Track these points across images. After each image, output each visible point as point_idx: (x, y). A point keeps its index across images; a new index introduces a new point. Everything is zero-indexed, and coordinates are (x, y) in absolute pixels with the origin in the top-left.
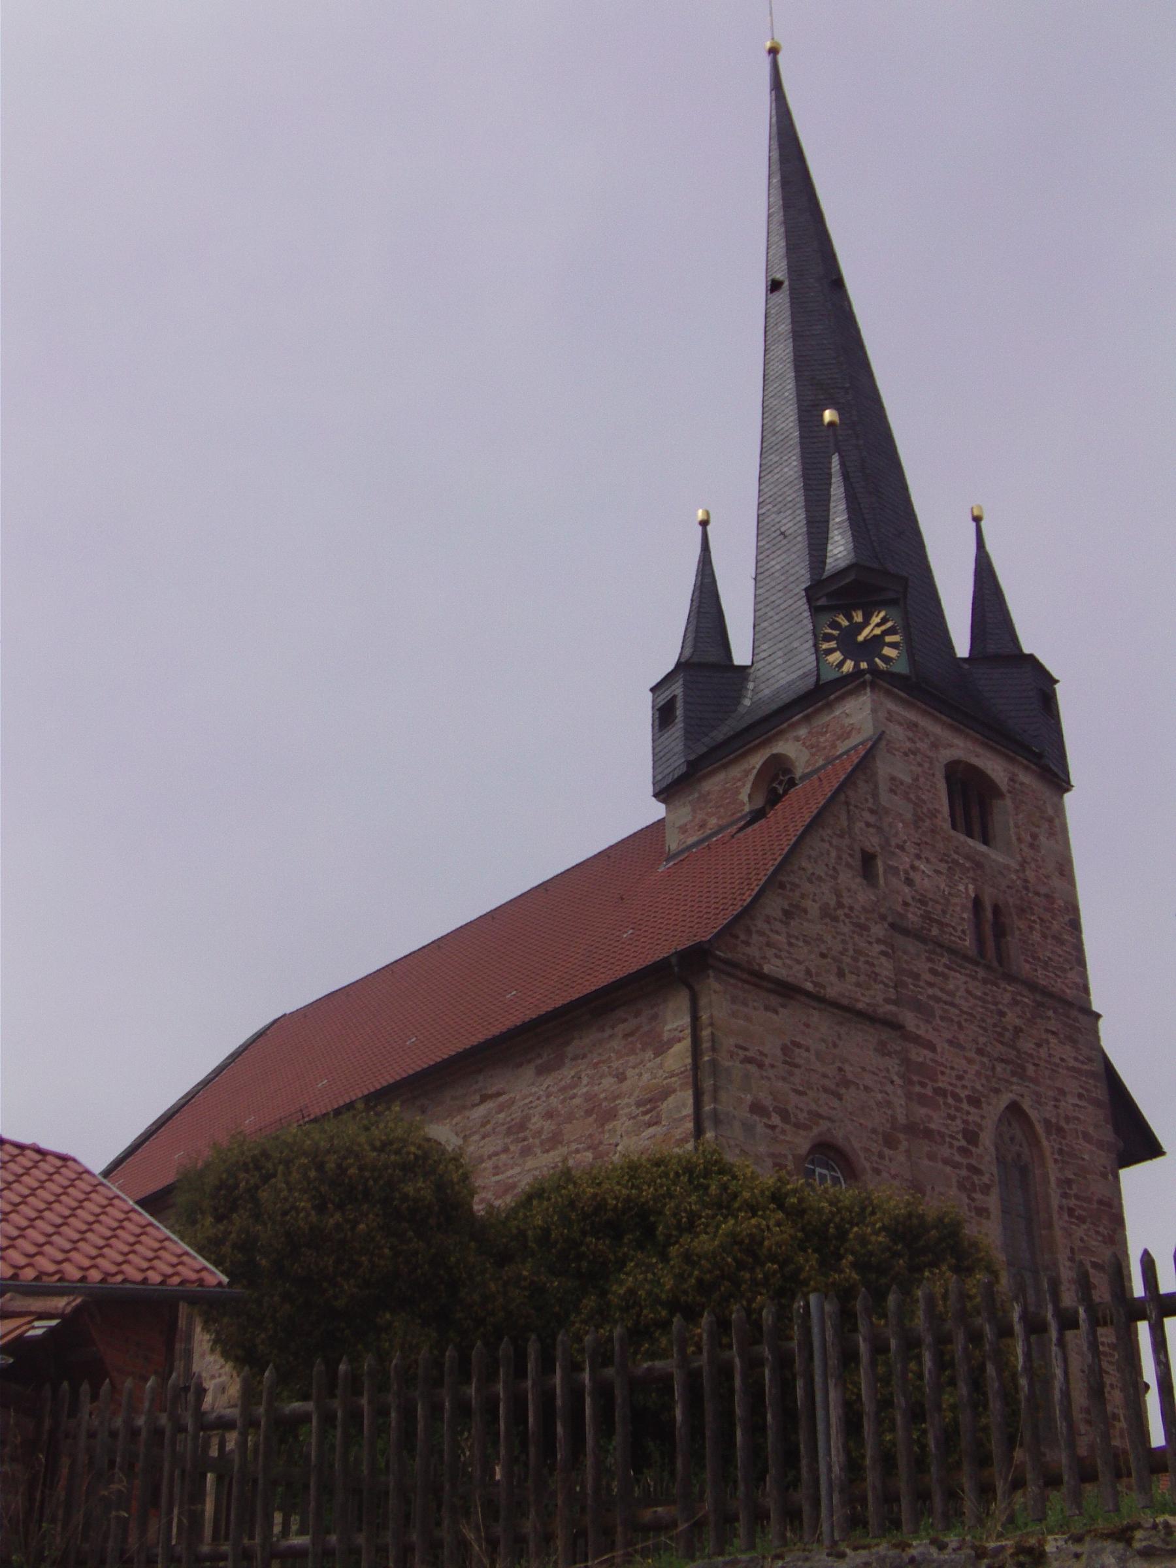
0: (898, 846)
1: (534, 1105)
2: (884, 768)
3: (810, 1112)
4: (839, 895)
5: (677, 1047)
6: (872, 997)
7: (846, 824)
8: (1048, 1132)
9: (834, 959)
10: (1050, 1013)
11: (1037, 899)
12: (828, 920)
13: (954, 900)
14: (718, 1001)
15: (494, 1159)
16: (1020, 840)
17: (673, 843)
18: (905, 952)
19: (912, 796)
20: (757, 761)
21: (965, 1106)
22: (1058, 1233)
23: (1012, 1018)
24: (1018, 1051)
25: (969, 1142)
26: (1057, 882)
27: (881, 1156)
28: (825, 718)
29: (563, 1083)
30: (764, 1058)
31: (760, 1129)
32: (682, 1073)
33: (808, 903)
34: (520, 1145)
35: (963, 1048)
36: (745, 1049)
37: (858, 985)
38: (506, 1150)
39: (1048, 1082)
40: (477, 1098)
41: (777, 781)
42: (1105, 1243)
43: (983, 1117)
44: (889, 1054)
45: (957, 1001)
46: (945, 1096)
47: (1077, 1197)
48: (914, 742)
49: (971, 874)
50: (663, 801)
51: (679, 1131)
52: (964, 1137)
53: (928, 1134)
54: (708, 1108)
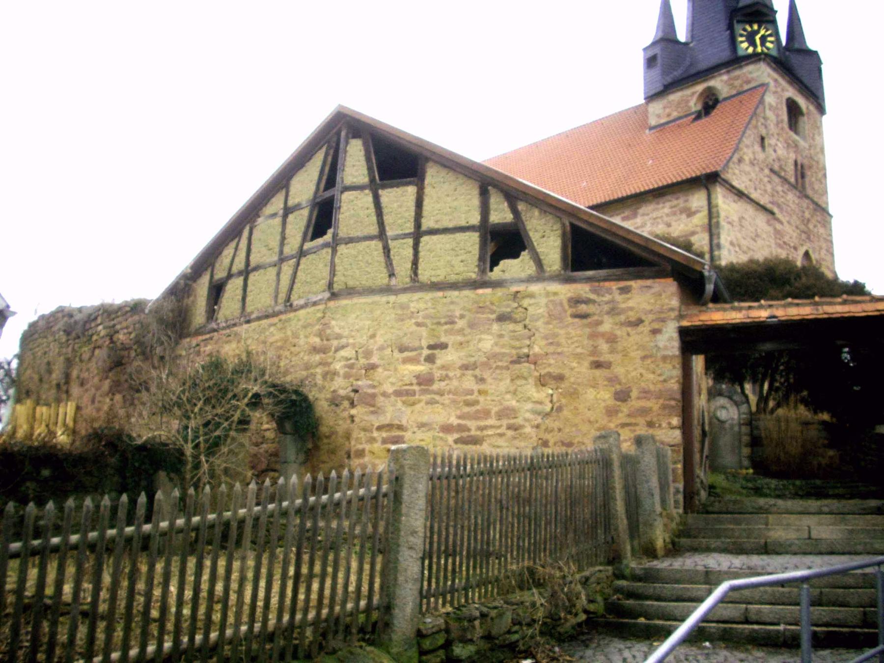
5: (698, 215)
6: (764, 200)
14: (720, 196)
23: (807, 215)
26: (828, 258)
28: (737, 73)
31: (733, 252)
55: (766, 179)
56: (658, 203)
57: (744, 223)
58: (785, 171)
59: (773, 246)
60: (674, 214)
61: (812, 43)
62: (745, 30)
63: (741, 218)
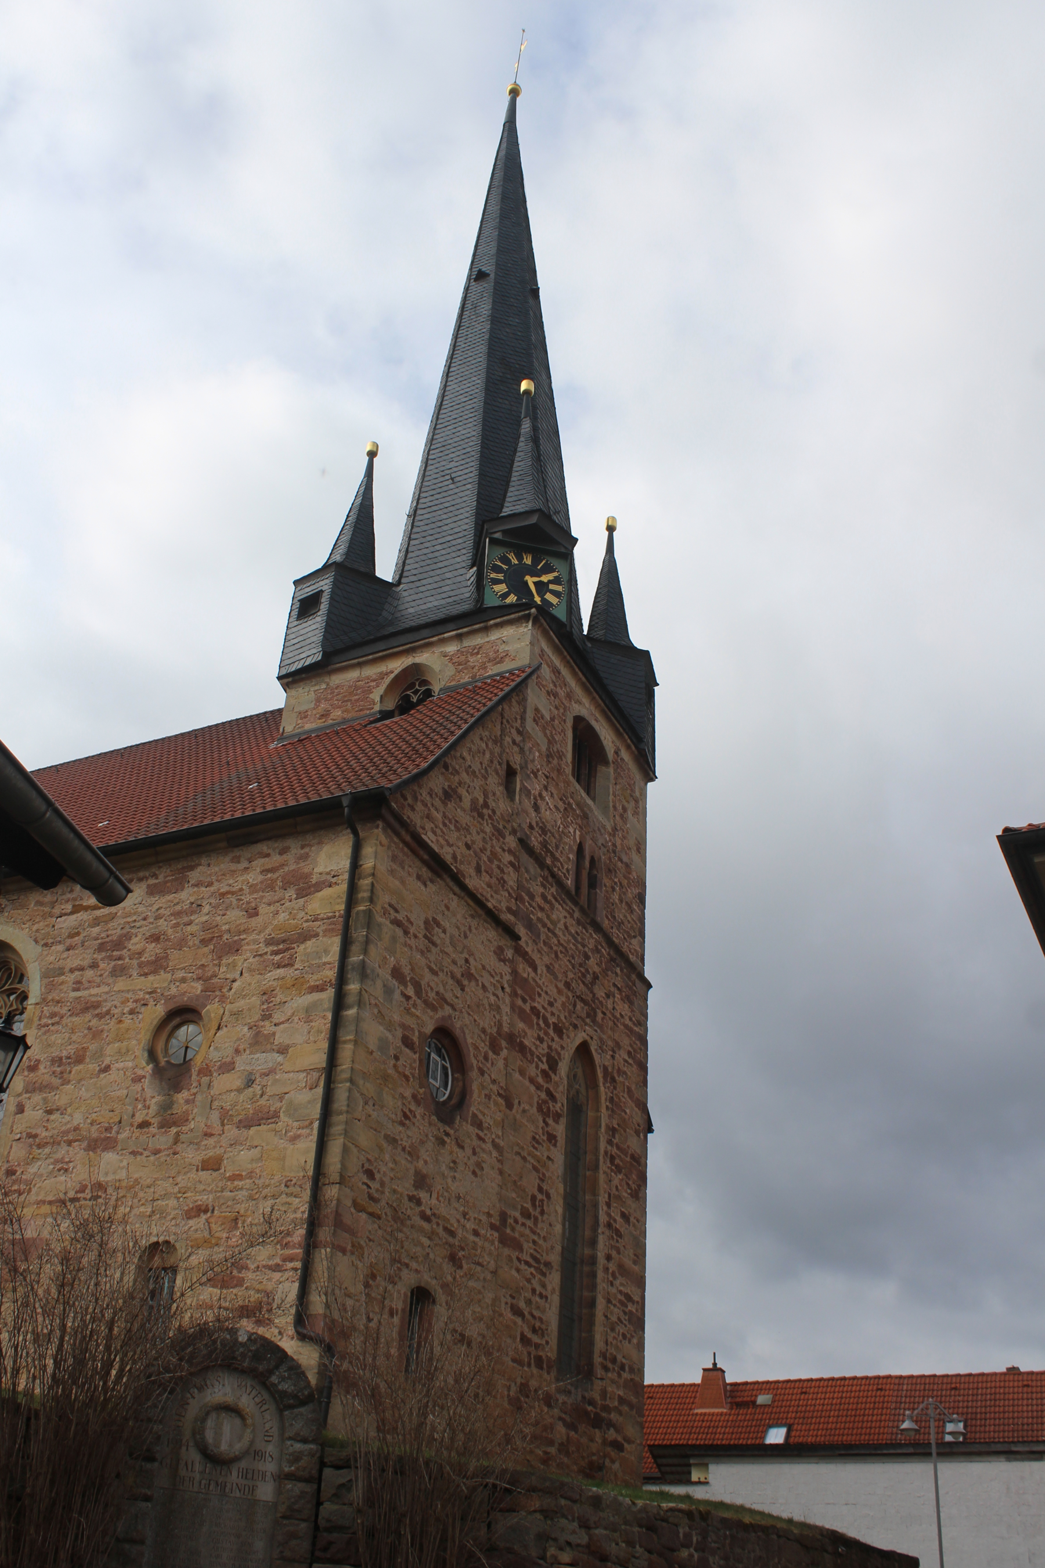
0: (533, 772)
1: (137, 924)
2: (536, 698)
3: (437, 993)
4: (486, 796)
5: (327, 892)
6: (498, 901)
7: (499, 733)
8: (605, 1077)
9: (475, 852)
10: (618, 970)
11: (619, 864)
12: (475, 814)
13: (567, 840)
15: (77, 973)
16: (614, 807)
17: (288, 726)
18: (527, 871)
19: (548, 732)
20: (397, 665)
21: (551, 1032)
22: (602, 1177)
24: (594, 995)
25: (550, 1068)
26: (635, 857)
27: (486, 1058)
28: (478, 640)
29: (178, 908)
30: (409, 926)
31: (397, 995)
32: (328, 918)
33: (462, 791)
34: (113, 963)
35: (556, 978)
36: (397, 911)
37: (489, 886)
38: (94, 966)
39: (610, 1032)
40: (69, 907)
41: (411, 692)
42: (632, 1196)
43: (563, 1048)
44: (504, 961)
45: (557, 931)
46: (538, 1018)
47: (618, 1148)
48: (555, 686)
49: (579, 821)
50: (286, 687)
51: (315, 977)
52: (547, 1061)
53: (522, 1049)
54: (355, 959)
55: (507, 858)
56: (237, 860)
57: (438, 935)
58: (555, 858)
59: (506, 1009)
60: (271, 887)
61: (639, 637)
62: (505, 560)
63: (431, 924)
